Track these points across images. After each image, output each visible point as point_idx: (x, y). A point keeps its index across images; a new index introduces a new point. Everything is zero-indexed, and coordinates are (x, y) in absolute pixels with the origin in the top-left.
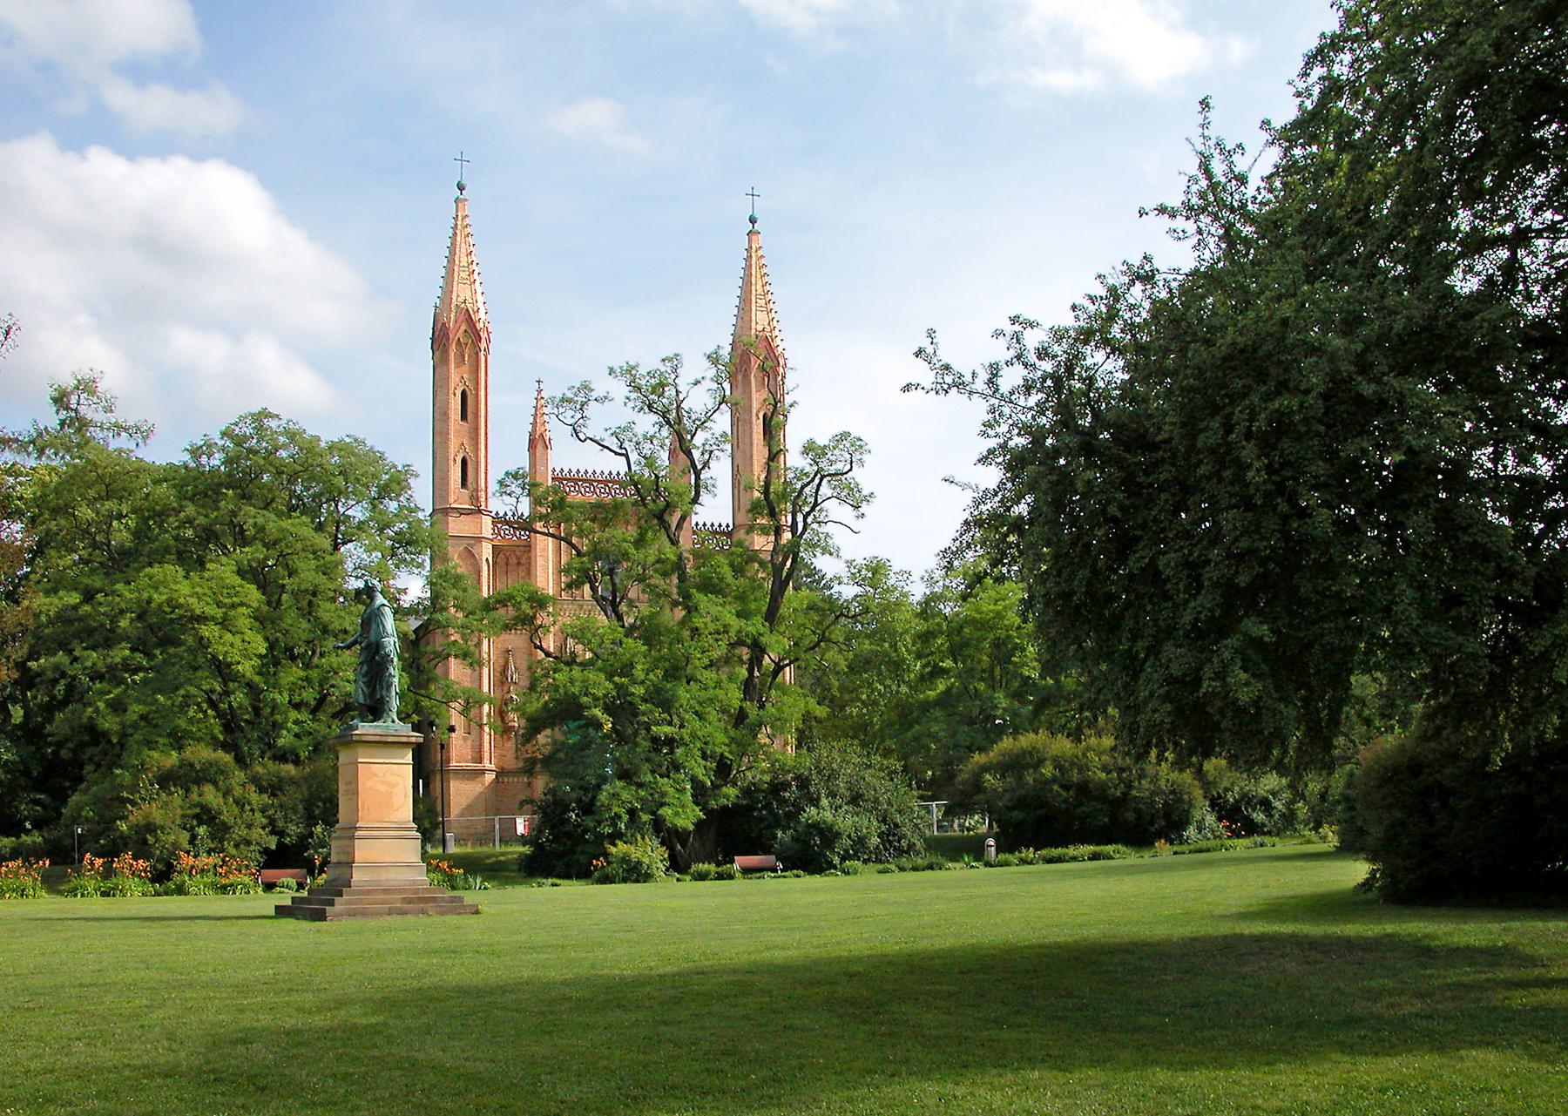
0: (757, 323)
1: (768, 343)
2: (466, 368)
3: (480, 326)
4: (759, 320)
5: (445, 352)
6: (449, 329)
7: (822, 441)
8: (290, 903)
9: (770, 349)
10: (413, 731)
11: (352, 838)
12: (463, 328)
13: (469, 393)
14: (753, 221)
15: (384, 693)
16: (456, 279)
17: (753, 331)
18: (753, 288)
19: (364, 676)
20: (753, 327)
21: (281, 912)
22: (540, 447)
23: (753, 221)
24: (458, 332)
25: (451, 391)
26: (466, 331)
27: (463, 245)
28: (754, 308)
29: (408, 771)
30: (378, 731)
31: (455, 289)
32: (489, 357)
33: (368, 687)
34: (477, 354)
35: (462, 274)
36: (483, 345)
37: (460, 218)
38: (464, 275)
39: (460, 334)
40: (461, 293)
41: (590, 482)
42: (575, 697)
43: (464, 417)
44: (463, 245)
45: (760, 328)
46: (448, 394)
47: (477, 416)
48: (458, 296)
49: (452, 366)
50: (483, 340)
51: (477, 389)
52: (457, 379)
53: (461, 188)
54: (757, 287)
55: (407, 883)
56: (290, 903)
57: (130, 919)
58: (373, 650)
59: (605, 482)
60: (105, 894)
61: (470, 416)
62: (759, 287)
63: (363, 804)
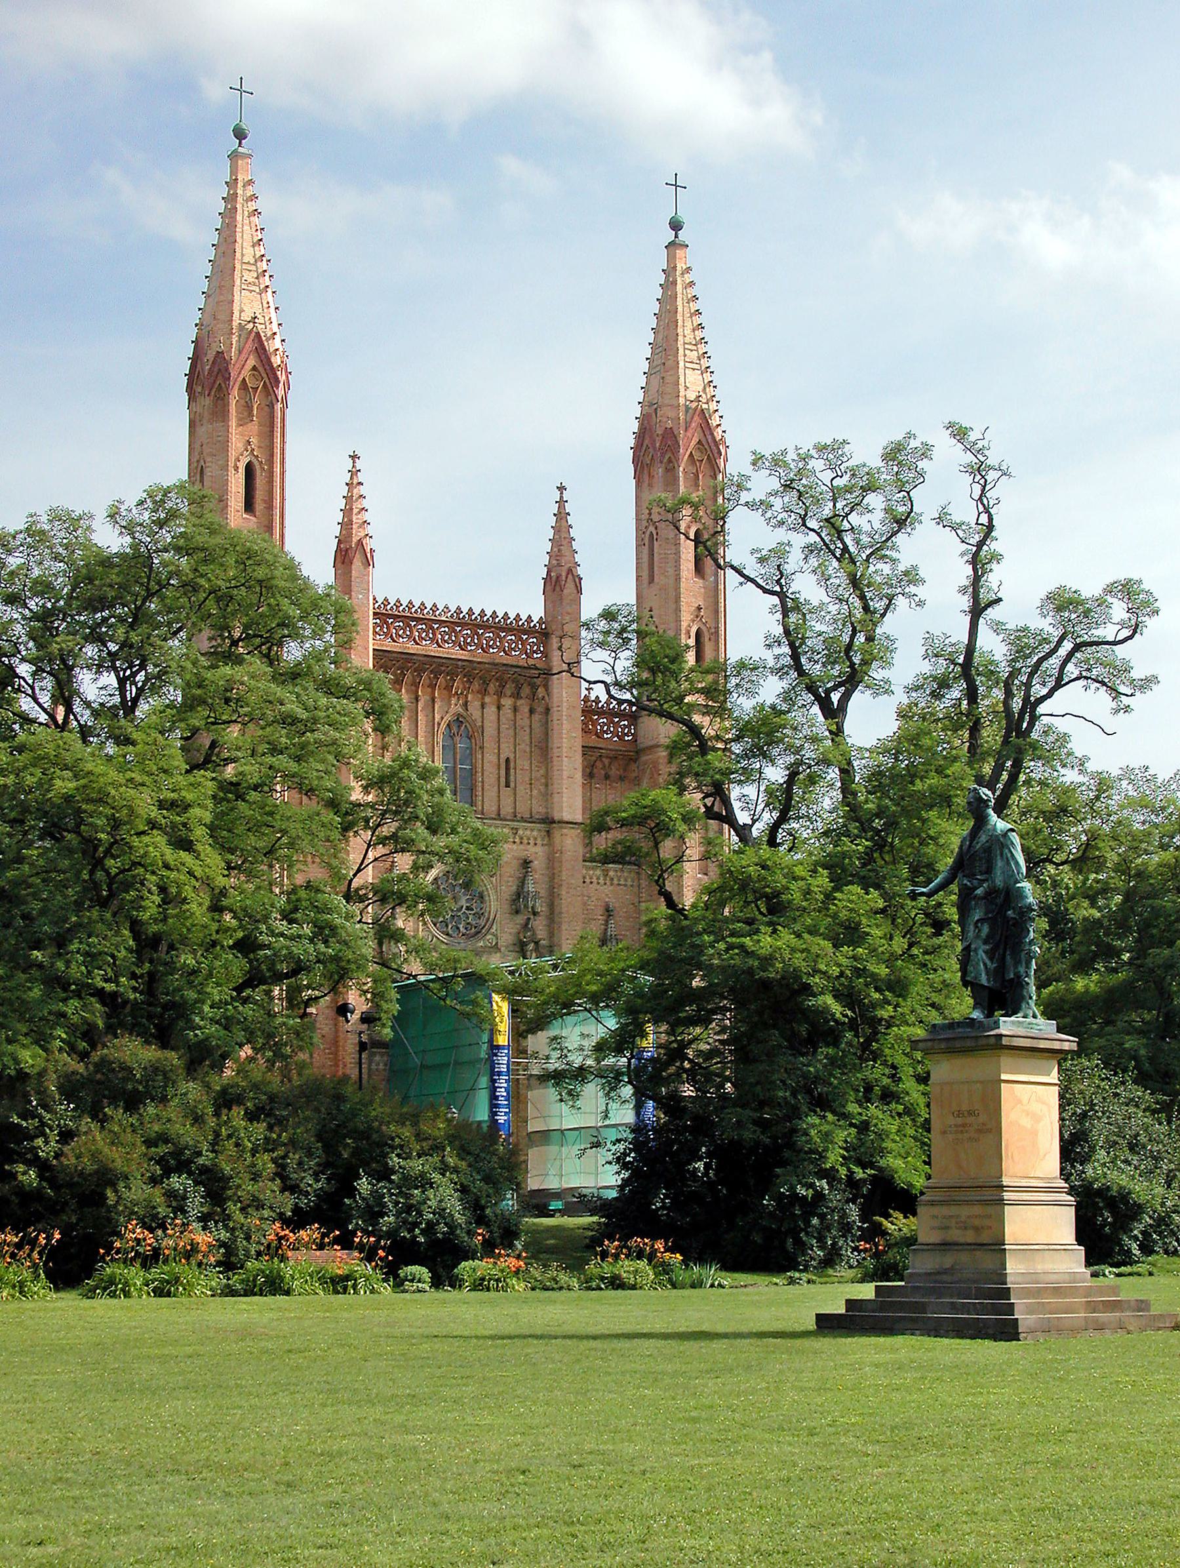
0: (686, 388)
1: (703, 420)
2: (254, 427)
3: (276, 361)
4: (691, 384)
5: (221, 398)
6: (228, 363)
7: (1090, 589)
8: (843, 1311)
9: (706, 428)
10: (1058, 1032)
11: (1001, 1202)
12: (252, 362)
13: (257, 466)
14: (676, 226)
15: (1022, 970)
16: (238, 282)
17: (682, 401)
18: (680, 330)
19: (985, 942)
20: (682, 393)
21: (827, 1324)
22: (357, 563)
23: (676, 226)
24: (243, 368)
25: (231, 464)
26: (254, 368)
27: (246, 228)
28: (681, 364)
29: (1052, 1096)
30: (1021, 1031)
31: (237, 298)
32: (287, 411)
33: (991, 959)
34: (271, 406)
35: (247, 276)
36: (280, 393)
37: (240, 184)
38: (250, 277)
39: (246, 373)
40: (245, 306)
41: (429, 622)
42: (796, 974)
43: (249, 506)
44: (246, 228)
45: (692, 396)
46: (225, 468)
47: (270, 507)
48: (242, 311)
49: (233, 423)
50: (281, 385)
51: (271, 462)
52: (241, 446)
53: (240, 134)
54: (685, 332)
55: (1067, 1277)
56: (843, 1311)
57: (618, 1336)
58: (999, 901)
59: (451, 624)
60: (159, 1292)
61: (259, 506)
62: (688, 331)
63: (1007, 1146)
